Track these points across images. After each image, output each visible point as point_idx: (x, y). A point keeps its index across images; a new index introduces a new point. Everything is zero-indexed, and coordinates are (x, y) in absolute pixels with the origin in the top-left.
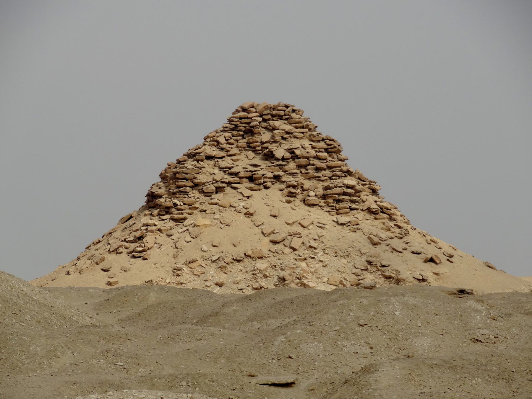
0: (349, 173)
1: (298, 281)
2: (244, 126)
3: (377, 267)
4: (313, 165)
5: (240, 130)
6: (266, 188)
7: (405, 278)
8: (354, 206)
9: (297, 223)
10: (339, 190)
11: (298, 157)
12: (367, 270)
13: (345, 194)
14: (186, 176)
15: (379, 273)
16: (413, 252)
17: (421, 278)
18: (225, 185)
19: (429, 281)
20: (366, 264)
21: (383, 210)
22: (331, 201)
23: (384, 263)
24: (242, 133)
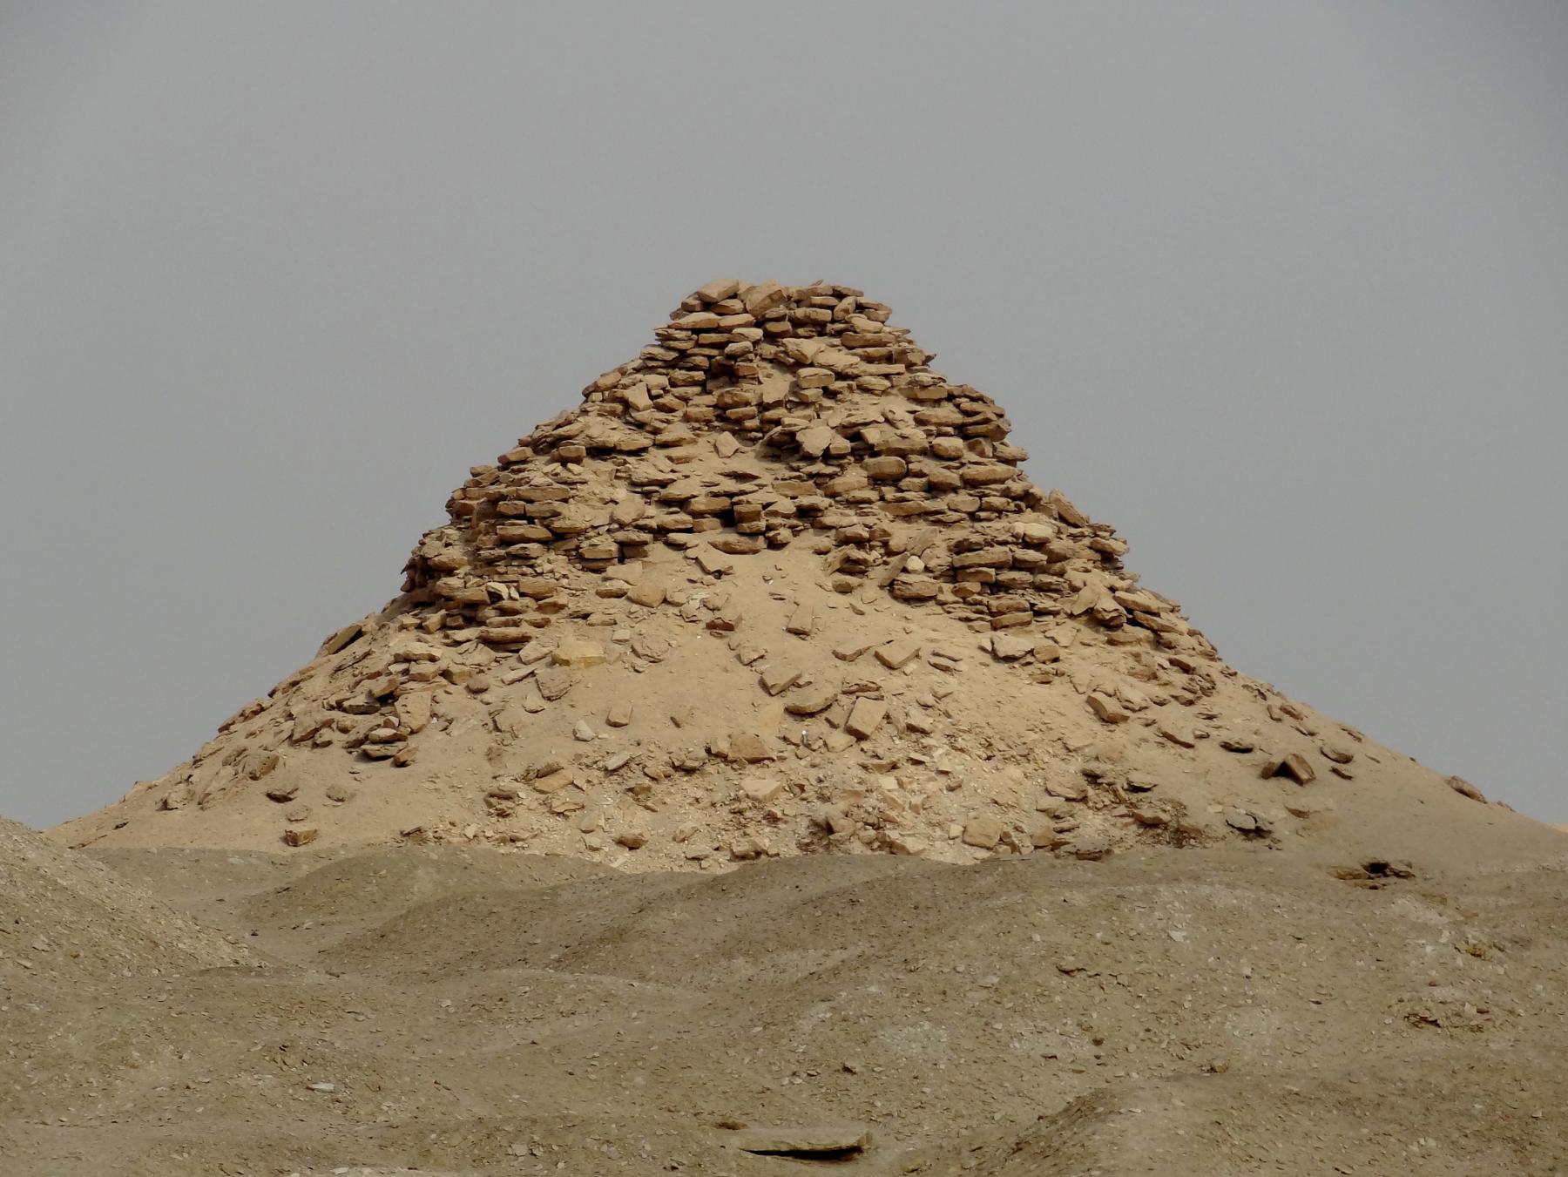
0: (1029, 501)
1: (872, 832)
2: (707, 356)
3: (1115, 792)
4: (920, 474)
5: (696, 368)
6: (775, 545)
7: (1201, 826)
8: (1044, 603)
9: (869, 656)
10: (998, 553)
11: (873, 451)
12: (1084, 800)
13: (1017, 565)
14: (529, 507)
15: (1122, 810)
16: (1227, 747)
17: (1251, 825)
18: (646, 537)
19: (1276, 835)
20: (1082, 781)
21: (1135, 615)
22: (973, 586)
23: (1138, 779)
24: (699, 375)
